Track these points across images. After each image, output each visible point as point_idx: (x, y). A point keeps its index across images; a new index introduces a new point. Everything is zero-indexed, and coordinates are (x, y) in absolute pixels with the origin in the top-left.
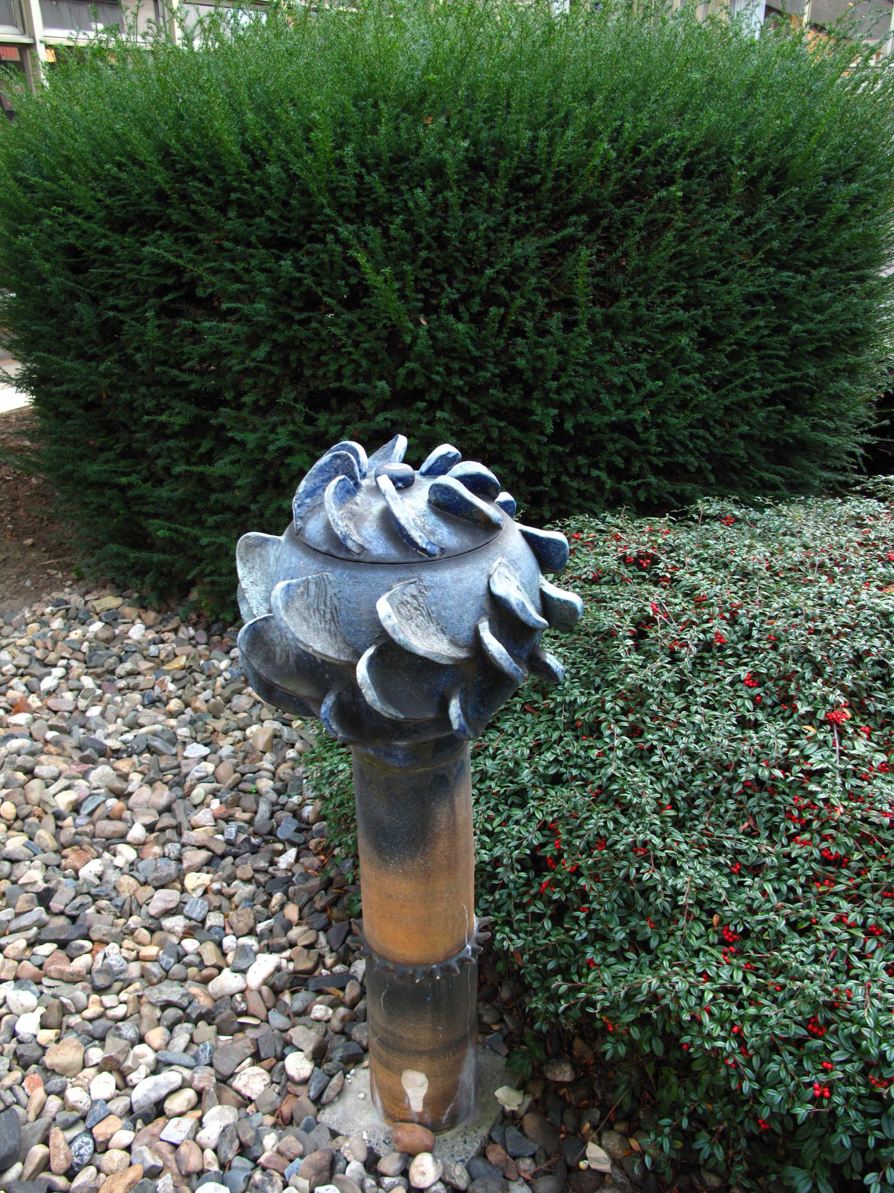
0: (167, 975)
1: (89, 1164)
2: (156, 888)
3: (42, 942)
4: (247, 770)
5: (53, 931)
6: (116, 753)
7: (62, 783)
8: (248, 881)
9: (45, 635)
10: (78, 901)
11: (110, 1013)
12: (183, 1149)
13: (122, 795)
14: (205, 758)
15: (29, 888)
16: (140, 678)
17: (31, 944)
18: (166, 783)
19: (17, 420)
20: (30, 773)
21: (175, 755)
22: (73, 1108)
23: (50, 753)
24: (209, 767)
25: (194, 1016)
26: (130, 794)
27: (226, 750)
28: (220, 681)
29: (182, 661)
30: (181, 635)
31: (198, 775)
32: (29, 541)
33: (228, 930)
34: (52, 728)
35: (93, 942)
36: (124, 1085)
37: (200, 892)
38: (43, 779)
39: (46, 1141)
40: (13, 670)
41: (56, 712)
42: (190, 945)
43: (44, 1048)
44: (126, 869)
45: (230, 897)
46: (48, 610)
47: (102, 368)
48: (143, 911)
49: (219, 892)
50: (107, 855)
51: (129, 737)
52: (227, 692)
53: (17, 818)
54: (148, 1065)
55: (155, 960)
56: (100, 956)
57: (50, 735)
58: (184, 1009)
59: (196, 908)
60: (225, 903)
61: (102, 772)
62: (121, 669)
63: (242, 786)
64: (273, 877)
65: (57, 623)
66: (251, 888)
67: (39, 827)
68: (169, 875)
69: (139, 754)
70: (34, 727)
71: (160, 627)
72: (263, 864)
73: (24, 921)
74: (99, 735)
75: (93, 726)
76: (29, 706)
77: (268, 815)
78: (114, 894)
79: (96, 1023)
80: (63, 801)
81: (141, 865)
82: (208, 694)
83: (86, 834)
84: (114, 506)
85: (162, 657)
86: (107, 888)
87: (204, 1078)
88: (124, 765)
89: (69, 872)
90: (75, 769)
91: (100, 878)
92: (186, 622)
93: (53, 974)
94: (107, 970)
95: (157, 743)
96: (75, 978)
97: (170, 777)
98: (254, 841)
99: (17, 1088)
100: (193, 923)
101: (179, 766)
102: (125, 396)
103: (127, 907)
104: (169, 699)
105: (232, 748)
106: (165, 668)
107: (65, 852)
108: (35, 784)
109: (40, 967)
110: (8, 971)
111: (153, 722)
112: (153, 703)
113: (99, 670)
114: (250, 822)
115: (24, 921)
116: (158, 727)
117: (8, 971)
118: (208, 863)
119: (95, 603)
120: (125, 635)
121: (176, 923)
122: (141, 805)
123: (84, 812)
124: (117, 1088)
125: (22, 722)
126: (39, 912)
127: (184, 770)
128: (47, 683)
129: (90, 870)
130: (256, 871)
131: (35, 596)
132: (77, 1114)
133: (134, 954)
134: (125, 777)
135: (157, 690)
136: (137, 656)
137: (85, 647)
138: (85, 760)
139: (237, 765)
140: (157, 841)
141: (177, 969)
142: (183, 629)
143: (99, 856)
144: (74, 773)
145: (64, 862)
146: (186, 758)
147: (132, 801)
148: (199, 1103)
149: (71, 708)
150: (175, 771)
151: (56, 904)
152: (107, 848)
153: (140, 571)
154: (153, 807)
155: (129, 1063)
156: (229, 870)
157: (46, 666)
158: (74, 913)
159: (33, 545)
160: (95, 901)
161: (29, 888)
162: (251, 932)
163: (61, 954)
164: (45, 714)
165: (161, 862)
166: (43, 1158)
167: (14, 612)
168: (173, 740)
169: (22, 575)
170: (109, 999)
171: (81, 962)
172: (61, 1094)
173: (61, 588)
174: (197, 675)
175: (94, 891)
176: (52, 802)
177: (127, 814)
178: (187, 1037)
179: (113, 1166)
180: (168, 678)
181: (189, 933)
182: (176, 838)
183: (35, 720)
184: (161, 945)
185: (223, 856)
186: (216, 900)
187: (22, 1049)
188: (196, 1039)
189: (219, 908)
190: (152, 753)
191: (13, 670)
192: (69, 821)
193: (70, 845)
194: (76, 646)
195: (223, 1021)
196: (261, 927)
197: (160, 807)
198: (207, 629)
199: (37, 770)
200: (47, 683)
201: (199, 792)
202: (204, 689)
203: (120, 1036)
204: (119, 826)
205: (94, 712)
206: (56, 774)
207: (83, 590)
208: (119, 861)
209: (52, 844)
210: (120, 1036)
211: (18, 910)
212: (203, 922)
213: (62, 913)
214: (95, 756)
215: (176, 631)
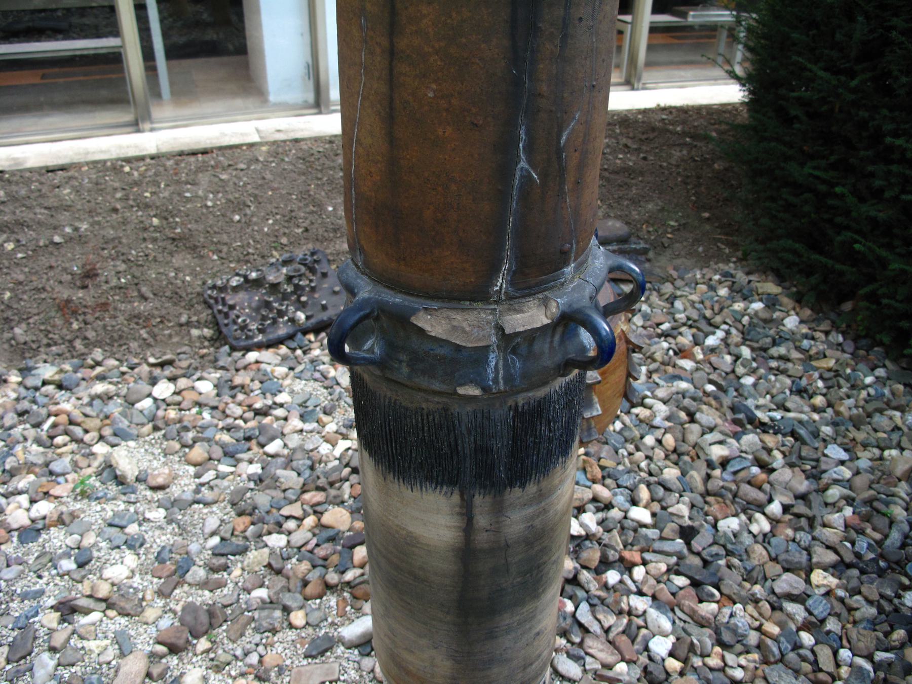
2: (786, 570)
3: (678, 573)
4: (882, 490)
5: (690, 567)
6: (763, 427)
8: (870, 602)
9: (712, 298)
10: (715, 549)
14: (842, 463)
15: (675, 519)
18: (804, 471)
19: (708, 113)
21: (816, 449)
23: (710, 405)
24: (847, 474)
27: (864, 463)
28: (864, 394)
29: (831, 363)
30: (830, 338)
31: (835, 476)
32: (706, 215)
33: (845, 642)
34: (711, 382)
35: (721, 594)
37: (823, 590)
38: (701, 426)
40: (684, 320)
41: (715, 369)
42: (807, 638)
44: (760, 538)
45: (850, 610)
46: (717, 277)
47: (854, 83)
49: (841, 600)
50: (743, 517)
51: (777, 415)
52: (870, 408)
53: (675, 451)
55: (775, 639)
56: (727, 611)
57: (710, 388)
59: (820, 608)
60: (844, 613)
61: (751, 439)
62: (774, 351)
63: (875, 504)
64: (896, 610)
65: (723, 292)
66: (873, 611)
67: (692, 468)
68: (799, 563)
69: (784, 435)
70: (697, 375)
71: (813, 325)
72: (889, 592)
73: (667, 546)
74: (750, 403)
75: (746, 394)
76: (693, 355)
77: (898, 544)
78: (745, 557)
79: (716, 674)
80: (717, 452)
81: (773, 541)
82: (851, 402)
84: (806, 208)
85: (812, 352)
86: (740, 548)
88: (770, 440)
89: (710, 518)
90: (729, 427)
91: (735, 535)
92: (835, 327)
93: (685, 609)
94: (734, 630)
95: (802, 432)
96: (704, 622)
97: (808, 467)
98: (882, 564)
100: (814, 620)
101: (817, 460)
102: (863, 114)
103: (755, 574)
104: (815, 393)
105: (870, 463)
106: (814, 363)
107: (709, 499)
108: (695, 428)
111: (799, 412)
112: (801, 392)
113: (755, 345)
114: (880, 543)
115: (667, 546)
116: (804, 417)
118: (834, 566)
119: (758, 285)
120: (780, 322)
122: (780, 483)
123: (731, 469)
125: (688, 368)
127: (823, 467)
128: (711, 341)
129: (730, 524)
130: (882, 596)
131: (704, 261)
133: (757, 624)
134: (769, 451)
135: (804, 382)
136: (791, 344)
137: (745, 320)
138: (736, 422)
139: (872, 482)
140: (789, 524)
141: (792, 656)
142: (833, 333)
143: (736, 515)
145: (706, 508)
146: (825, 455)
147: (774, 476)
149: (728, 370)
150: (814, 463)
152: (744, 511)
153: (808, 271)
154: (791, 490)
156: (854, 583)
157: (711, 325)
158: (709, 558)
159: (708, 219)
161: (675, 519)
162: (869, 657)
163: (692, 591)
164: (708, 369)
167: (687, 270)
168: (816, 434)
169: (697, 241)
170: (730, 658)
171: (708, 609)
173: (727, 261)
174: (842, 381)
175: (729, 546)
176: (707, 448)
177: (767, 487)
180: (816, 375)
181: (806, 626)
182: (807, 528)
183: (697, 369)
184: (781, 625)
185: (849, 566)
186: (838, 608)
189: (838, 615)
190: (796, 439)
191: (684, 320)
192: (717, 472)
193: (715, 495)
194: (738, 317)
196: (880, 656)
197: (797, 493)
198: (855, 340)
199: (698, 416)
200: (711, 341)
201: (834, 493)
202: (849, 397)
205: (749, 381)
206: (712, 425)
207: (747, 269)
208: (755, 528)
209: (701, 487)
211: (664, 535)
213: (698, 554)
214: (745, 422)
215: (827, 333)
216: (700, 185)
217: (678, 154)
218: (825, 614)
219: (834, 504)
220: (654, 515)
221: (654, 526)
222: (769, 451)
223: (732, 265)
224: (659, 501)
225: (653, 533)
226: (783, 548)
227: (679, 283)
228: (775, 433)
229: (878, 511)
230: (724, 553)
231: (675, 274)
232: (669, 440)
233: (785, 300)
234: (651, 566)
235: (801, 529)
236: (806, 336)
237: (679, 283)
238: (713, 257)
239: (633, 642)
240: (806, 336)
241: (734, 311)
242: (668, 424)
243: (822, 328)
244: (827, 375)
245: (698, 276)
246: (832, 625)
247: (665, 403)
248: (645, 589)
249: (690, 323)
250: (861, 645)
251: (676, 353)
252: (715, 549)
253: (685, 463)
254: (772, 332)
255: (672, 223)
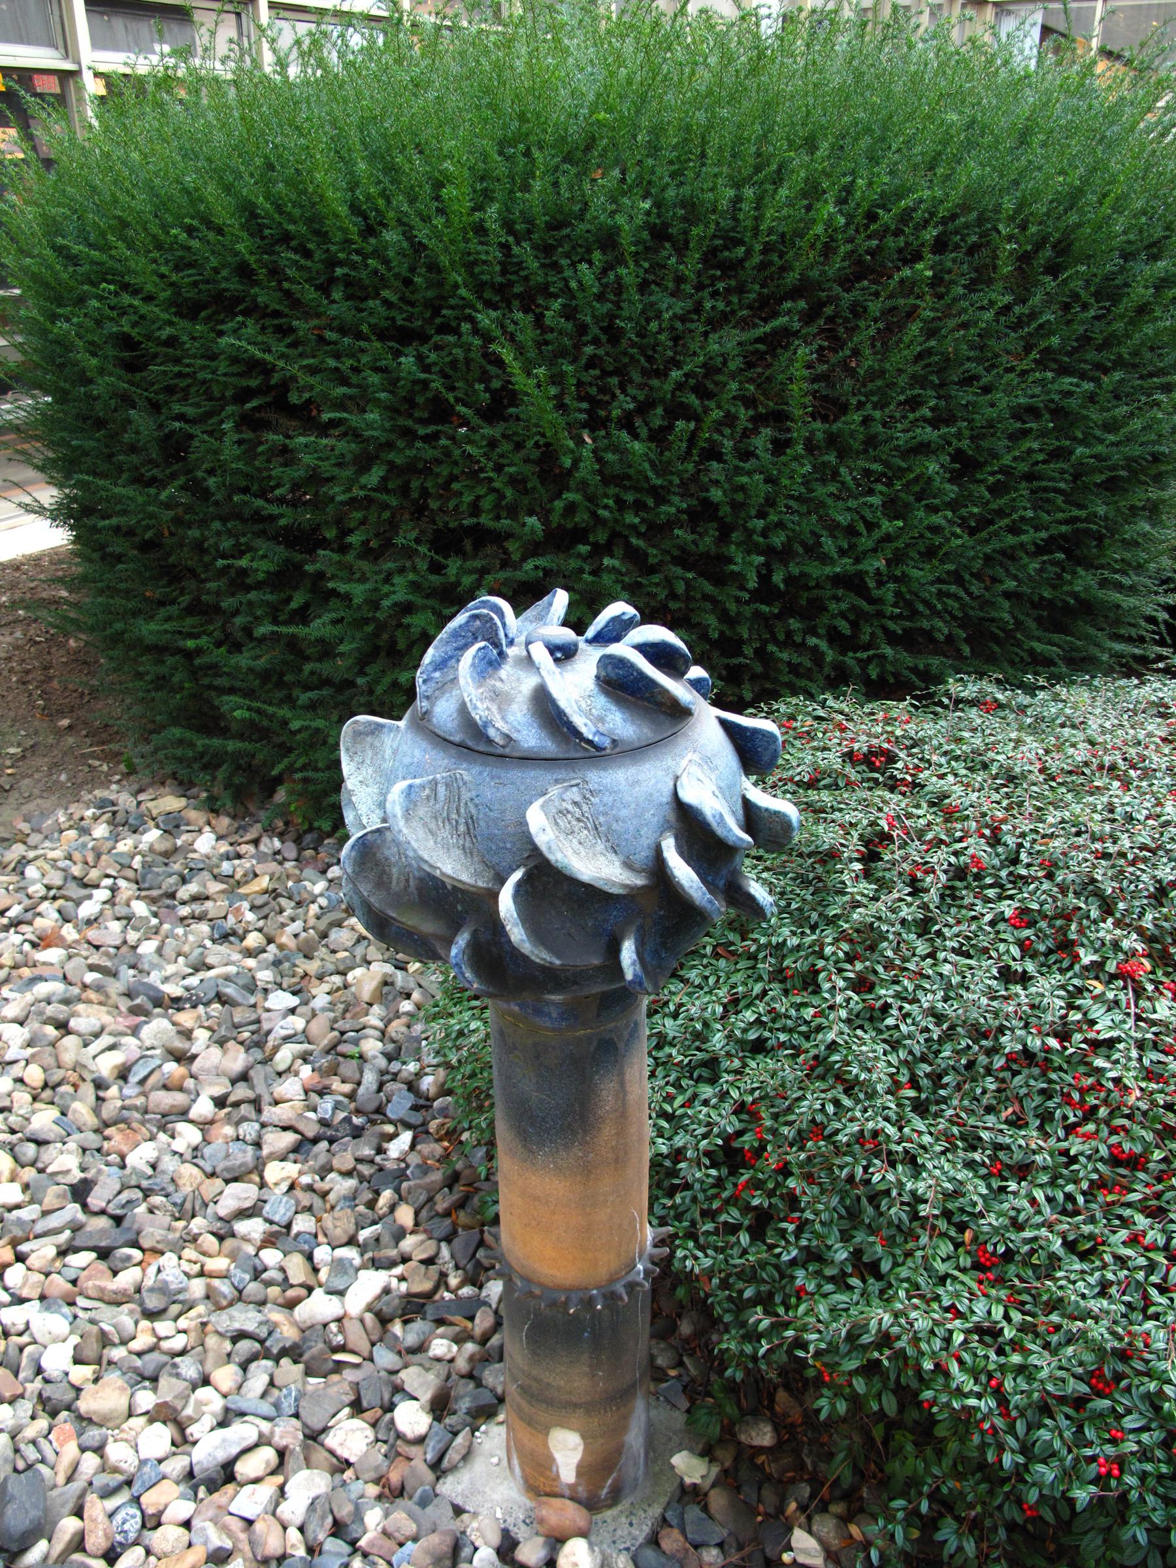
0: (239, 1295)
1: (136, 1543)
2: (227, 1182)
3: (76, 1250)
4: (347, 1027)
7: (106, 1040)
8: (348, 1174)
9: (84, 845)
10: (125, 1196)
11: (165, 1345)
12: (259, 1527)
13: (183, 1058)
14: (293, 1011)
15: (60, 1179)
16: (209, 904)
17: (62, 1253)
20: (63, 1026)
21: (254, 1006)
22: (116, 1470)
23: (89, 1002)
25: (275, 1351)
26: (194, 1057)
27: (321, 999)
28: (314, 909)
29: (264, 882)
30: (262, 848)
31: (284, 1033)
32: (65, 722)
33: (321, 1238)
34: (92, 968)
35: (143, 1250)
36: (183, 1441)
37: (284, 1187)
39: (79, 1513)
40: (43, 892)
41: (97, 947)
42: (271, 1257)
43: (78, 1390)
45: (324, 1195)
46: (89, 813)
47: (164, 496)
48: (210, 1210)
49: (310, 1188)
50: (163, 1137)
52: (322, 925)
53: (46, 1085)
54: (13, 1498)
55: (225, 1276)
56: (152, 1270)
57: (90, 977)
58: (262, 1342)
60: (317, 1202)
61: (158, 1028)
62: (184, 893)
63: (340, 1048)
65: (101, 831)
67: (74, 1099)
69: (207, 1004)
70: (69, 967)
71: (236, 838)
72: (368, 1151)
73: (54, 1221)
74: (154, 978)
75: (146, 967)
76: (62, 939)
77: (375, 1087)
78: (171, 1188)
79: (147, 1357)
80: (106, 1065)
81: (207, 1151)
82: (297, 926)
83: (136, 1108)
85: (238, 876)
87: (288, 1433)
88: (186, 1018)
90: (122, 1023)
91: (154, 1166)
92: (269, 830)
93: (91, 1293)
94: (162, 1289)
95: (230, 990)
96: (119, 1298)
97: (246, 1035)
99: (42, 1442)
100: (275, 1228)
102: (194, 533)
103: (188, 1206)
104: (247, 931)
105: (328, 998)
106: (242, 891)
107: (108, 1132)
108: (70, 1041)
109: (74, 1282)
110: (33, 1287)
111: (226, 961)
112: (225, 937)
113: (155, 893)
114: (351, 1096)
115: (54, 1221)
116: (232, 969)
117: (33, 1287)
118: (296, 1149)
120: (189, 847)
121: (253, 1228)
122: (208, 1072)
123: (134, 1079)
124: (173, 1444)
126: (73, 1210)
127: (266, 1026)
128: (88, 909)
129: (140, 1156)
130: (359, 1160)
131: (72, 793)
132: (120, 1478)
134: (187, 1034)
136: (206, 875)
137: (137, 862)
138: (135, 1011)
139: (335, 1021)
140: (228, 1119)
141: (253, 1288)
143: (152, 1138)
144: (121, 1028)
145: (106, 1145)
147: (196, 1066)
148: (281, 1465)
150: (253, 1027)
151: (96, 1200)
152: (163, 1128)
153: (211, 763)
155: (189, 1411)
157: (86, 886)
158: (119, 1212)
159: (70, 727)
160: (146, 1196)
161: (60, 1179)
162: (351, 1241)
163: (102, 1266)
164: (84, 950)
165: (234, 1147)
166: (75, 1535)
167: (44, 815)
169: (55, 766)
170: (164, 1327)
171: (127, 1278)
172: (99, 1450)
173: (106, 784)
174: (283, 902)
175: (145, 1184)
177: (190, 1083)
178: (265, 1379)
179: (167, 1547)
181: (269, 1241)
182: (253, 1115)
184: (233, 1256)
185: (315, 1141)
186: (306, 1199)
187: (48, 1391)
188: (277, 1382)
189: (309, 1209)
190: (223, 1003)
192: (113, 1091)
193: (115, 1123)
195: (313, 1358)
196: (364, 1234)
197: (233, 1075)
199: (73, 1023)
200: (88, 909)
201: (284, 1056)
202: (293, 920)
203: (178, 1375)
204: (178, 1098)
206: (97, 1028)
207: (136, 787)
208: (179, 1145)
209: (91, 1121)
210: (178, 1375)
212: (288, 1226)
213: (103, 1212)
214: (149, 1006)
215: (256, 842)
216: (50, 679)
217: (8, 639)
218: (290, 1214)
219: (288, 1070)
220: (26, 1187)
221: (32, 1201)
222: (187, 1034)
223: (114, 787)
224: (33, 1164)
225: (29, 1213)
226: (222, 1155)
227: (34, 839)
228: (194, 1007)
229: (345, 1056)
230: (140, 1195)
231: (25, 827)
232: (35, 1075)
233: (193, 814)
234: (32, 1261)
235: (244, 1119)
236: (227, 857)
237: (34, 839)
238: (85, 782)
239: (16, 1375)
240: (227, 857)
241: (121, 854)
242: (30, 1051)
243: (249, 836)
244: (260, 901)
245: (62, 819)
246: (303, 1224)
247: (21, 1024)
248: (25, 1293)
249: (53, 894)
250: (339, 1231)
251: (34, 945)
252: (125, 1196)
253: (62, 1096)
254: (177, 867)
255: (12, 750)
